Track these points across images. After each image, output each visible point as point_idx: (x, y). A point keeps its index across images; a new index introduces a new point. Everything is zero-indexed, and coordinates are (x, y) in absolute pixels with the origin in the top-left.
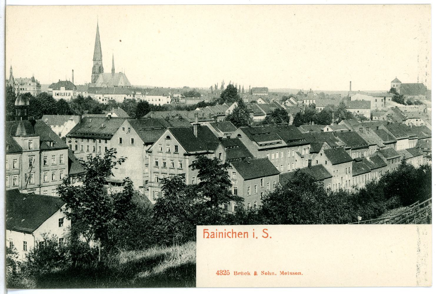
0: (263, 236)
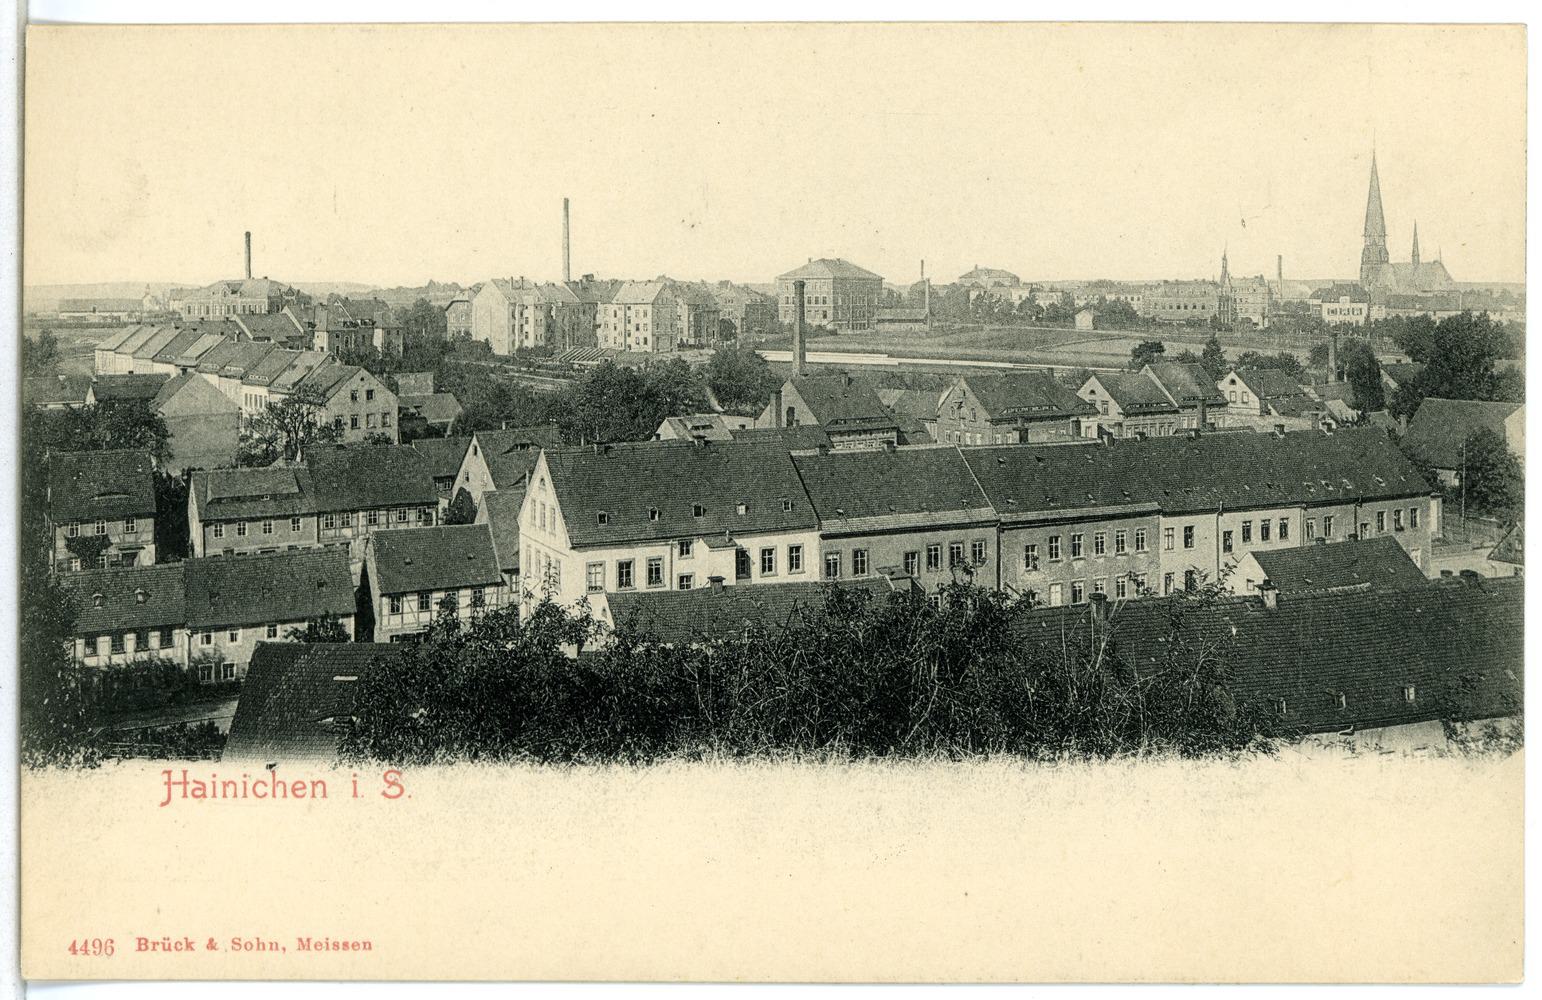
0: (163, 804)
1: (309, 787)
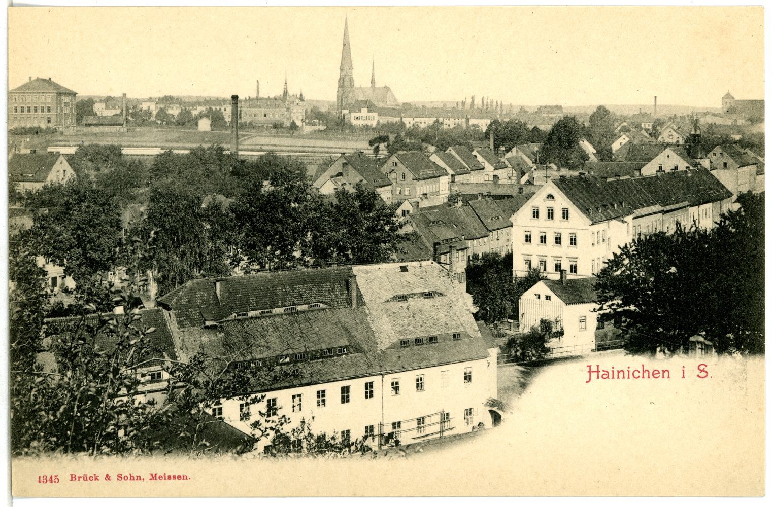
0: (587, 382)
1: (661, 372)
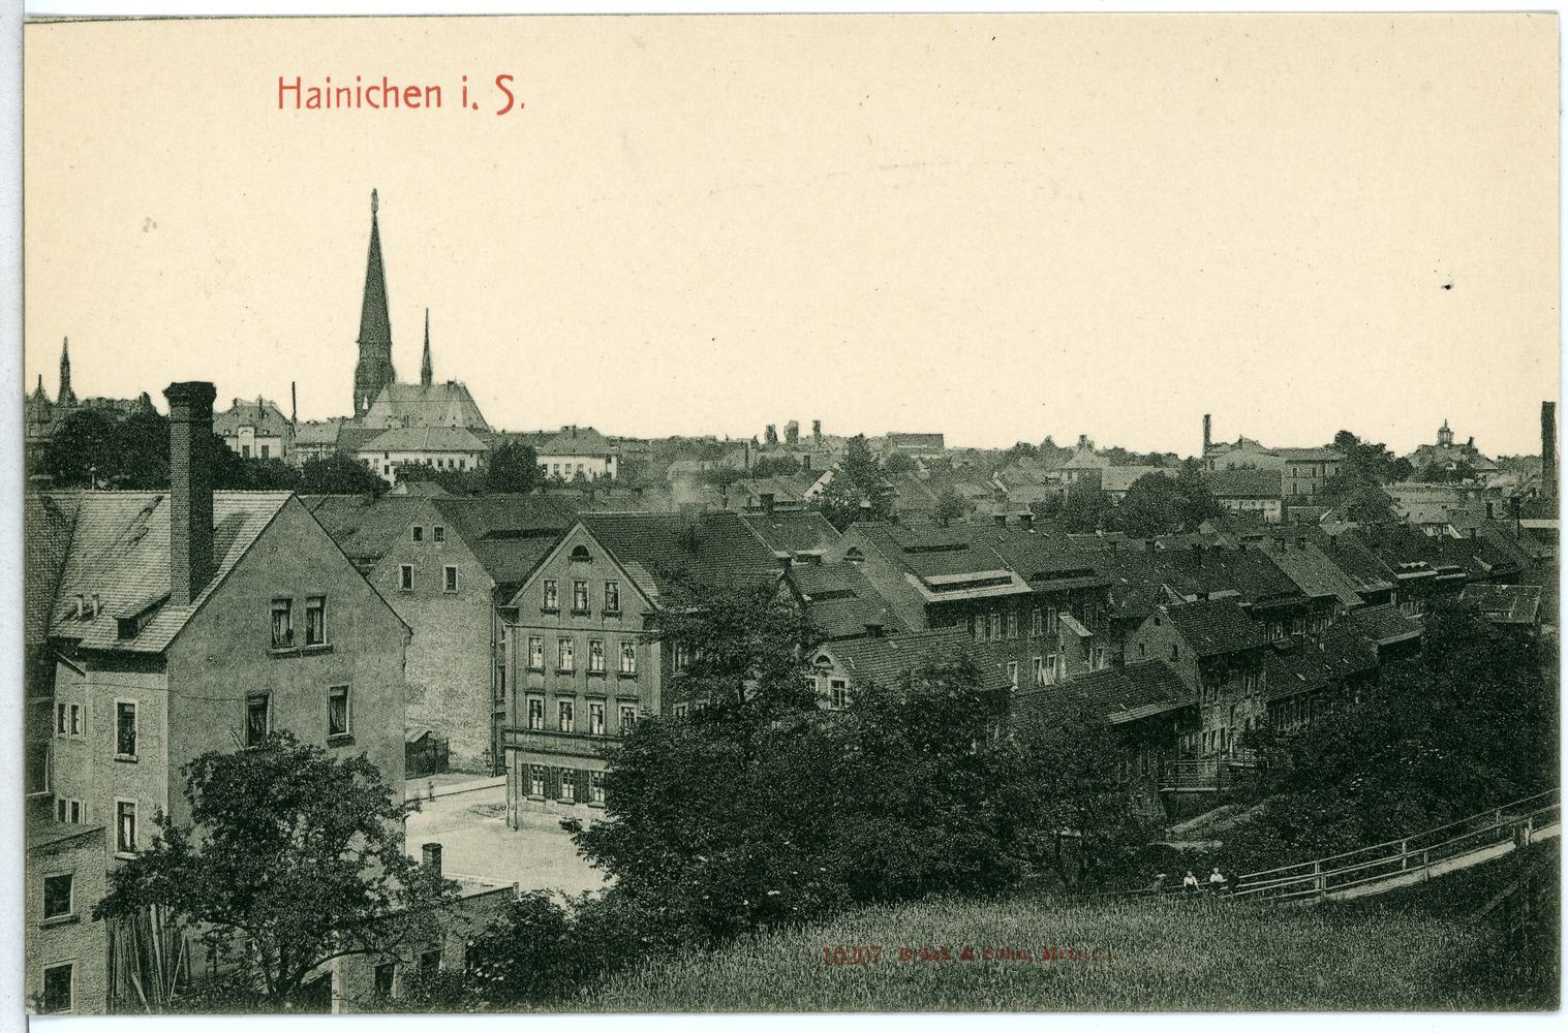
0: (500, 113)
